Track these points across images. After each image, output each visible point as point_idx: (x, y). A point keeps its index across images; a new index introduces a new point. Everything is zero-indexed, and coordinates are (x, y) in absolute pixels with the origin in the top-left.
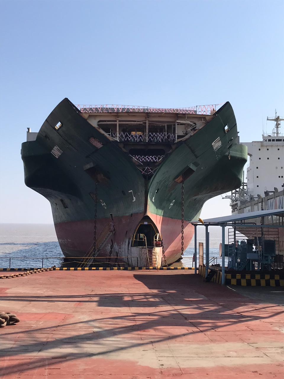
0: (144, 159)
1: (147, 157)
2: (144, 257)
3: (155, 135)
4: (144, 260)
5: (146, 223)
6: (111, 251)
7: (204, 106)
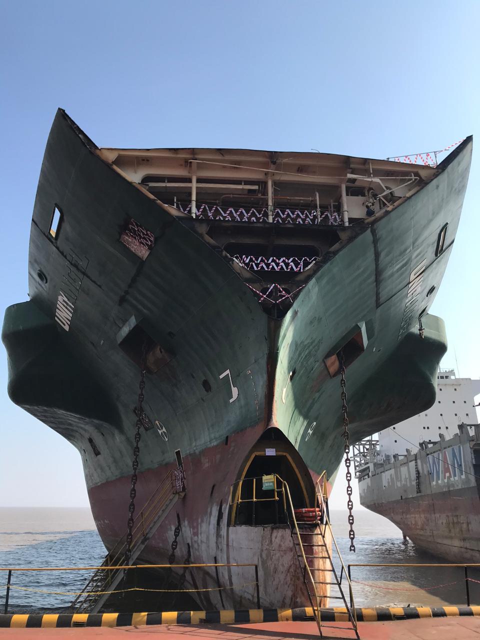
0: (265, 264)
1: (273, 261)
2: (283, 565)
3: (291, 214)
4: (282, 577)
5: (270, 452)
6: (175, 541)
7: (406, 157)
